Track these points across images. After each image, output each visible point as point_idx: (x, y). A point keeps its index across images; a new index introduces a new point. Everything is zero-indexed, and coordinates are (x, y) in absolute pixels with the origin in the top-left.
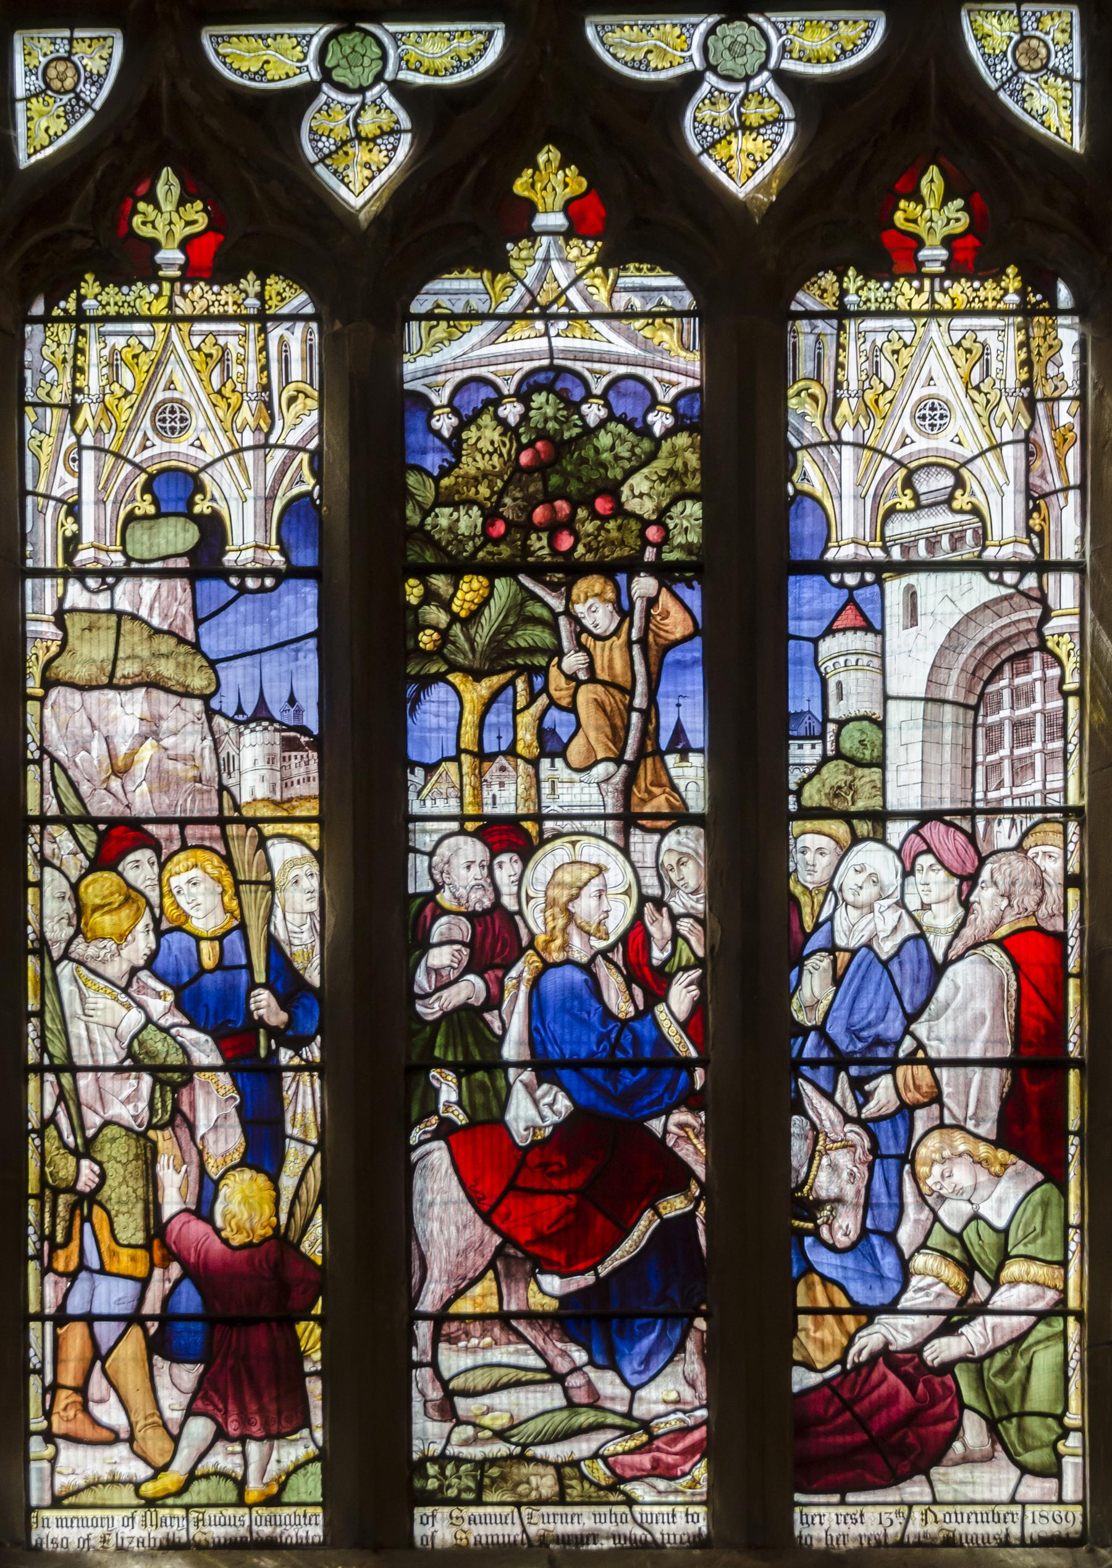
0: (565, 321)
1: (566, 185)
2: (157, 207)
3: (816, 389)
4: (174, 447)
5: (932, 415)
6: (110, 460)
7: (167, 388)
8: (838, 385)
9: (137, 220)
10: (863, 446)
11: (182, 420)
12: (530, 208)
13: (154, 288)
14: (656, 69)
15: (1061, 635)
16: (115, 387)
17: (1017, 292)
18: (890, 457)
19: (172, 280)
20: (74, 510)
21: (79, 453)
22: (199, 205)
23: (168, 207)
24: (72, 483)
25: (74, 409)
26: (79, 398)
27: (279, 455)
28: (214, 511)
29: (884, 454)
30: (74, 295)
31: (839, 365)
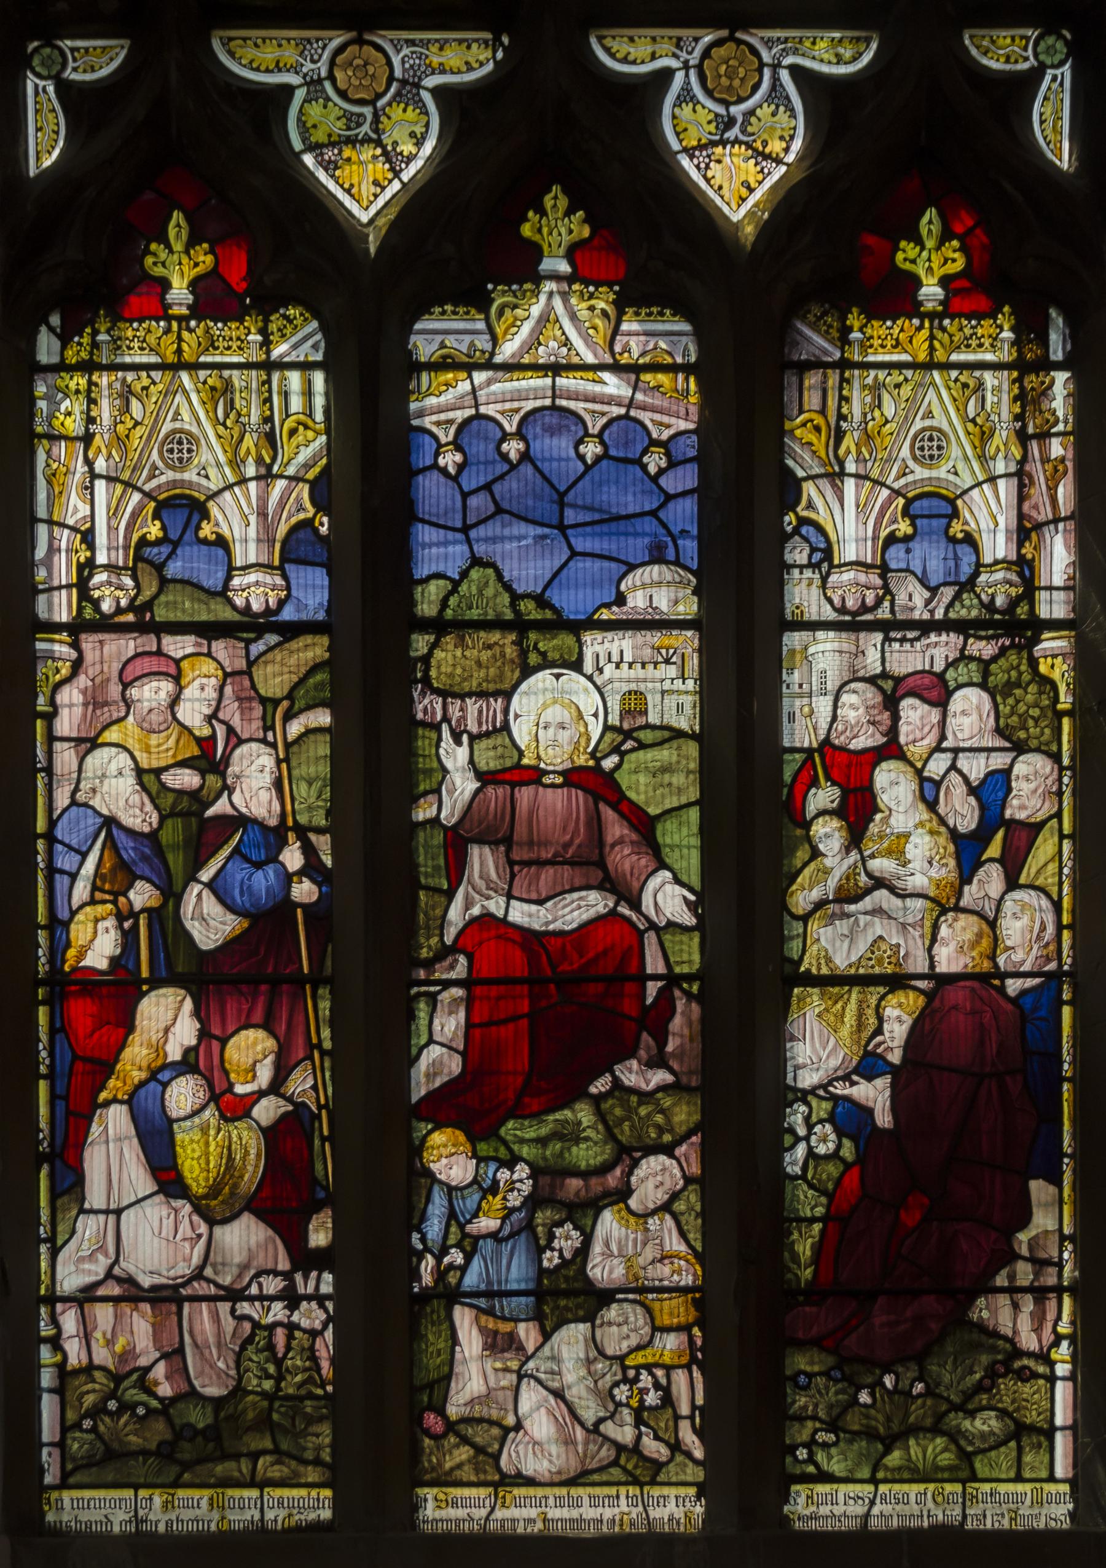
0: (556, 357)
1: (571, 232)
2: (168, 246)
3: (819, 420)
4: (934, 474)
5: (931, 444)
6: (119, 488)
7: (174, 420)
8: (841, 417)
9: (149, 260)
10: (866, 477)
11: (939, 448)
12: (535, 252)
13: (916, 322)
14: (58, 124)
15: (1054, 656)
16: (127, 418)
17: (850, 329)
18: (140, 490)
19: (180, 319)
20: (88, 537)
21: (92, 482)
22: (955, 243)
23: (178, 247)
24: (84, 510)
25: (87, 439)
26: (92, 428)
27: (281, 484)
28: (218, 534)
29: (883, 485)
30: (88, 330)
31: (843, 399)
